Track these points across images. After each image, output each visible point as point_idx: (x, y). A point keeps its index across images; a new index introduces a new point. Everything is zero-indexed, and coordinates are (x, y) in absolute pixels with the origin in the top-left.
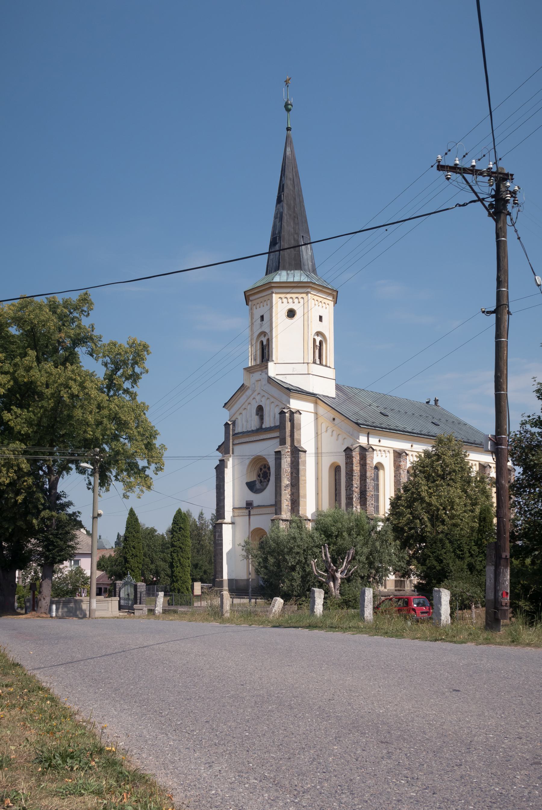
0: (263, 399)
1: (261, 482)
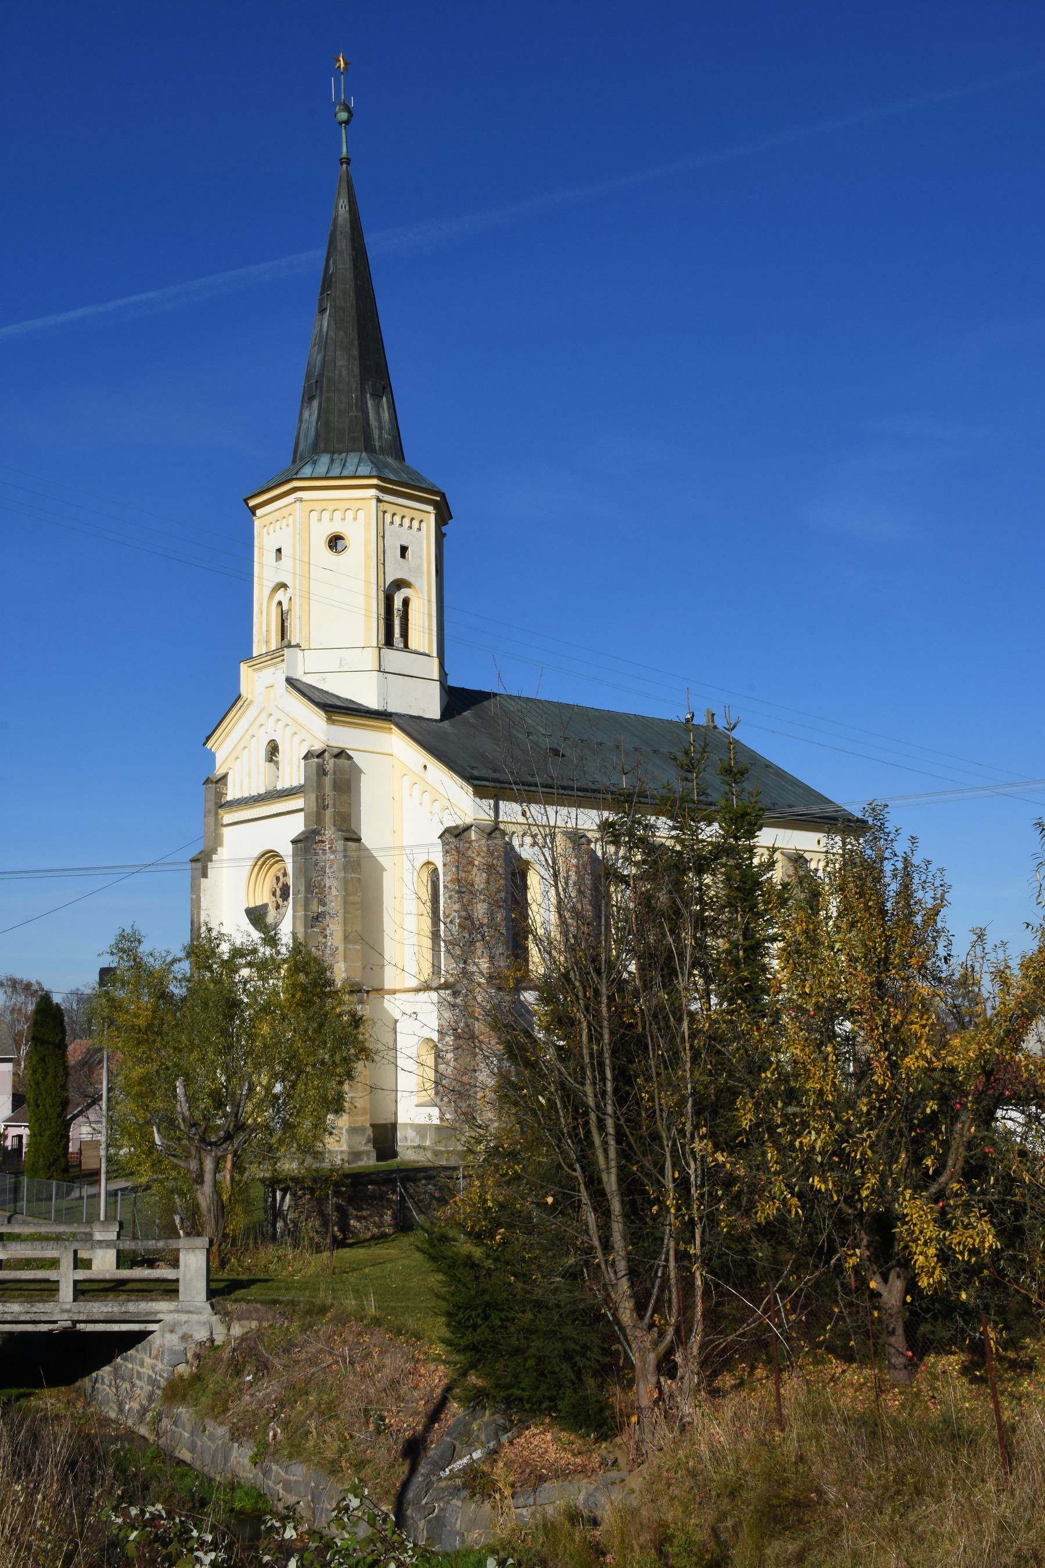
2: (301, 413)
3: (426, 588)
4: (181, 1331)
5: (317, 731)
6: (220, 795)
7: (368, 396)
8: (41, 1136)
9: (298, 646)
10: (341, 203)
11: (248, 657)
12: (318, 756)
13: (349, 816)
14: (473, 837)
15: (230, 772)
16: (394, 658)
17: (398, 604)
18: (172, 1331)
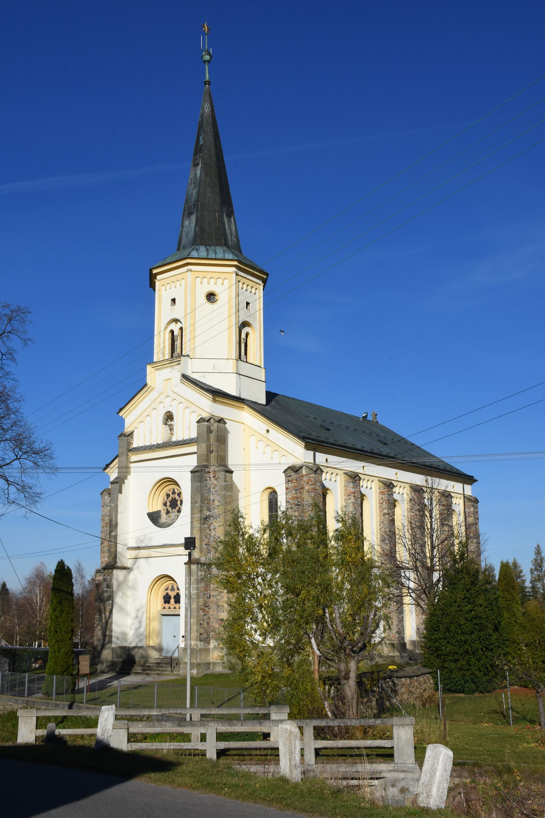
0: (175, 403)
1: (168, 512)
2: (183, 222)
3: (258, 328)
4: (400, 785)
5: (207, 406)
6: (129, 444)
7: (225, 215)
8: (59, 652)
9: (188, 356)
10: (206, 106)
11: (151, 362)
12: (208, 421)
13: (225, 457)
14: (304, 473)
15: (136, 430)
16: (244, 368)
17: (243, 336)
18: (393, 786)
